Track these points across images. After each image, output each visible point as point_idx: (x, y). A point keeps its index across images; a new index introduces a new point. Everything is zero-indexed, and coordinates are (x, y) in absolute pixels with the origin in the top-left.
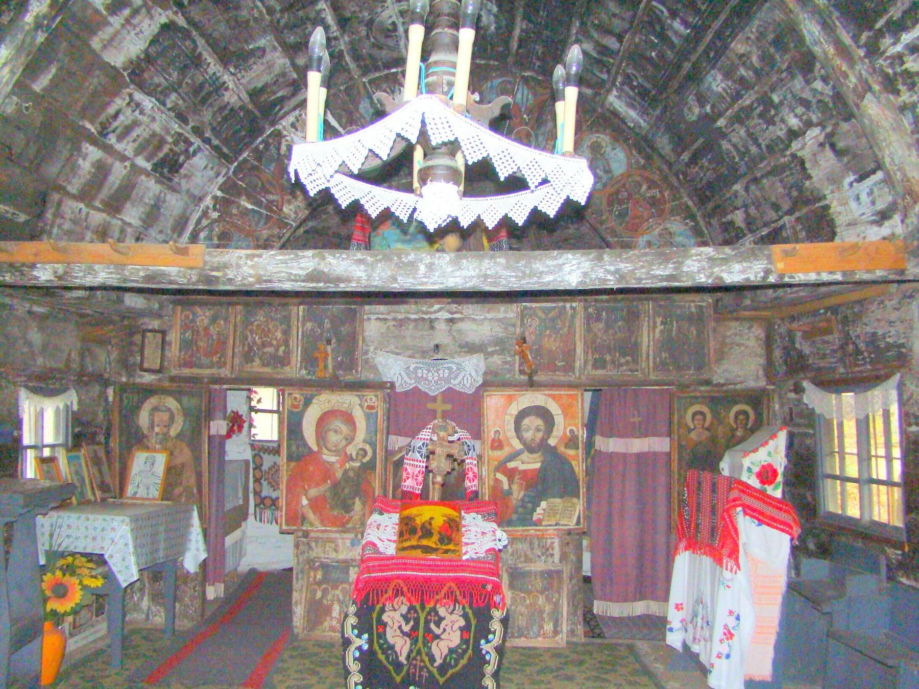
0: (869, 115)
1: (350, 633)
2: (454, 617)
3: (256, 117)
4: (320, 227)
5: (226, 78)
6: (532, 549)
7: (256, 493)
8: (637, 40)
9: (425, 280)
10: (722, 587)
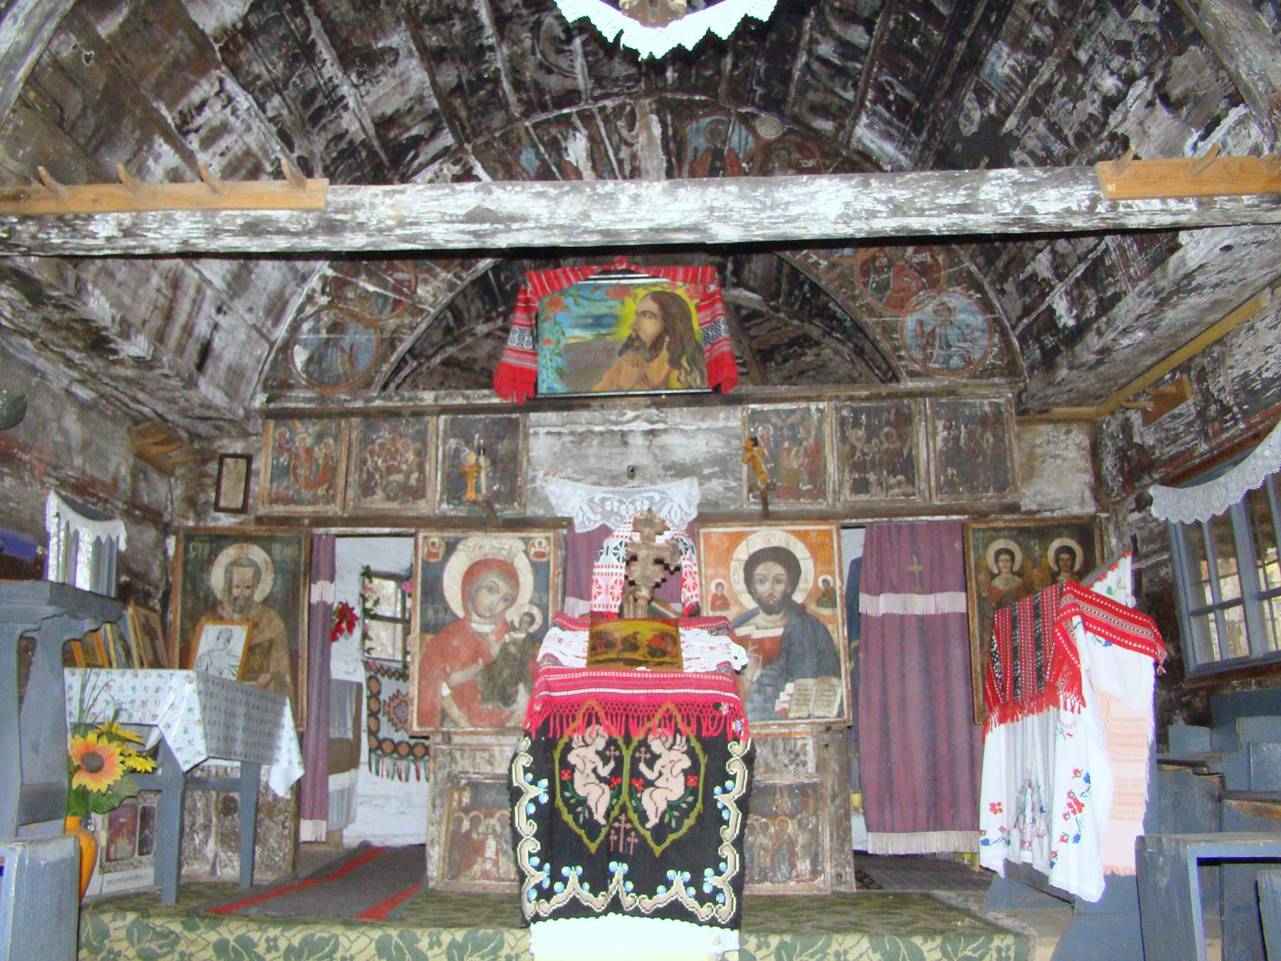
0: (1213, 14)
1: (520, 779)
2: (675, 755)
3: (382, 162)
4: (463, 357)
5: (345, 89)
6: (776, 755)
7: (372, 733)
8: (892, 24)
9: (628, 216)
10: (1060, 738)
